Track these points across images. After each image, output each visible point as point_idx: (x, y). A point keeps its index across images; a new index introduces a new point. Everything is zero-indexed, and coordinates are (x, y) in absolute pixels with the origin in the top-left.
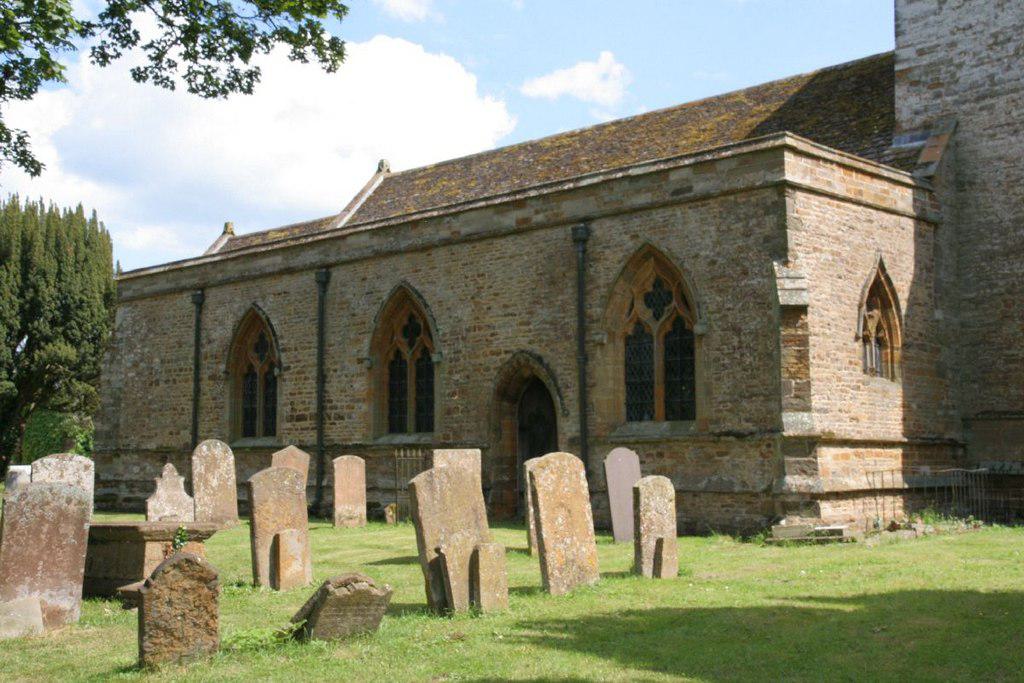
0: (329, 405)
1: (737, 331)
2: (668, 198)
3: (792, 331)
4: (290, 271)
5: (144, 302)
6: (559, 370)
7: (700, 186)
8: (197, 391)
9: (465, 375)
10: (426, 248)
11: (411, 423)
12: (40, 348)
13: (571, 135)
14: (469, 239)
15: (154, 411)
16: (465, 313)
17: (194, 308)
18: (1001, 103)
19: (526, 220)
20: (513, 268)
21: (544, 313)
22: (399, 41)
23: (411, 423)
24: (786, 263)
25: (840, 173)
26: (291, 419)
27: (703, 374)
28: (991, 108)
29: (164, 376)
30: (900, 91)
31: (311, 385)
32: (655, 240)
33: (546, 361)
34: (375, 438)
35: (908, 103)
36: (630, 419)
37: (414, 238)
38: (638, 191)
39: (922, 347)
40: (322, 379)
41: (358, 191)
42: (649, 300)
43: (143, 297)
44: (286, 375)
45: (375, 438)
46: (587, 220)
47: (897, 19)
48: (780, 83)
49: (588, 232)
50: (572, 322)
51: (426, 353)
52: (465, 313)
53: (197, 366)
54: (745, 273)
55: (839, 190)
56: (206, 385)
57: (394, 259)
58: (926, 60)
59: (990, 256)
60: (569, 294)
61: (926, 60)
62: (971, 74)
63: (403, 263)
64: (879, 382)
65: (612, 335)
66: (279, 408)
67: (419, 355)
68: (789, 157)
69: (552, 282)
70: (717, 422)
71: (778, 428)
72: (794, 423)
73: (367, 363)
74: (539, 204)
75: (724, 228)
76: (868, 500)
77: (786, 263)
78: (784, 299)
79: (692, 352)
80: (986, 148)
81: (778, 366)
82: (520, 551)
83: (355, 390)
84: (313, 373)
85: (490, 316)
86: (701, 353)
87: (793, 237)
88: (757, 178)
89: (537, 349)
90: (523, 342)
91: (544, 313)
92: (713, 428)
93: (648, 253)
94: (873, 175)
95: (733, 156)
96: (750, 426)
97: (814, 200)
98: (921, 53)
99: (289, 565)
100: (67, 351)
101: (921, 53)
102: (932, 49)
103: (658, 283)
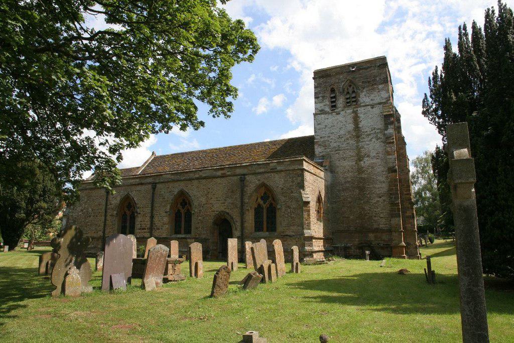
0: (154, 225)
1: (289, 207)
2: (269, 170)
3: (306, 208)
4: (142, 184)
5: (86, 191)
6: (234, 217)
7: (279, 168)
8: (105, 219)
9: (202, 220)
10: (190, 180)
11: (183, 231)
12: (35, 204)
13: (216, 149)
14: (205, 178)
15: (88, 225)
16: (203, 200)
17: (106, 194)
18: (341, 152)
19: (225, 174)
20: (220, 188)
21: (229, 201)
22: (404, 133)
23: (183, 231)
24: (304, 190)
25: (312, 167)
26: (140, 229)
27: (279, 219)
28: (338, 153)
29: (93, 214)
30: (316, 147)
31: (148, 219)
32: (266, 182)
33: (230, 214)
34: (170, 235)
35: (318, 150)
36: (255, 231)
37: (187, 177)
38: (260, 168)
39: (326, 214)
40: (152, 217)
41: (146, 160)
42: (262, 198)
43: (86, 189)
44: (139, 215)
45: (170, 235)
46: (244, 175)
47: (315, 128)
48: (278, 141)
49: (245, 178)
50: (239, 204)
51: (133, 213)
52: (203, 200)
53: (106, 212)
54: (292, 192)
55: (312, 171)
56: (108, 218)
57: (179, 182)
58: (322, 140)
59: (339, 191)
60: (238, 195)
61: (322, 140)
62: (333, 145)
63: (182, 184)
64: (319, 222)
65: (251, 207)
66: (136, 226)
67: (131, 214)
68: (304, 162)
69: (233, 192)
70: (283, 232)
71: (303, 234)
72: (307, 233)
73: (168, 213)
74: (229, 170)
75: (286, 180)
76: (318, 253)
77: (304, 190)
78: (304, 200)
79: (275, 213)
80: (337, 163)
81: (303, 218)
82: (244, 268)
83: (163, 220)
84: (149, 215)
85: (210, 201)
86: (278, 214)
87: (306, 183)
88: (296, 167)
89: (227, 211)
90: (222, 209)
91: (229, 201)
92: (282, 234)
93: (264, 185)
94: (318, 168)
95: (289, 161)
96: (293, 234)
97: (309, 174)
98: (321, 138)
99: (200, 271)
100: (45, 205)
101: (321, 138)
102: (324, 137)
103: (265, 193)
